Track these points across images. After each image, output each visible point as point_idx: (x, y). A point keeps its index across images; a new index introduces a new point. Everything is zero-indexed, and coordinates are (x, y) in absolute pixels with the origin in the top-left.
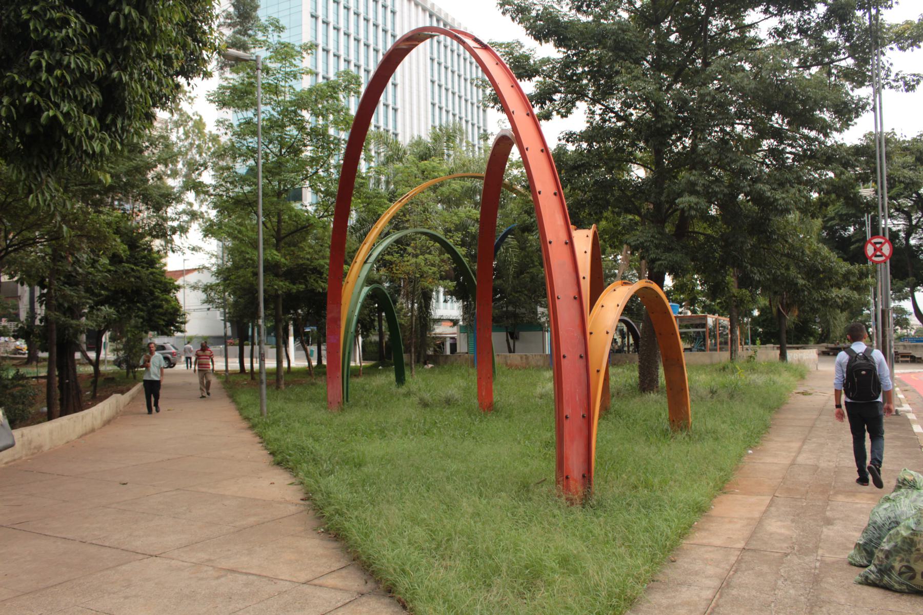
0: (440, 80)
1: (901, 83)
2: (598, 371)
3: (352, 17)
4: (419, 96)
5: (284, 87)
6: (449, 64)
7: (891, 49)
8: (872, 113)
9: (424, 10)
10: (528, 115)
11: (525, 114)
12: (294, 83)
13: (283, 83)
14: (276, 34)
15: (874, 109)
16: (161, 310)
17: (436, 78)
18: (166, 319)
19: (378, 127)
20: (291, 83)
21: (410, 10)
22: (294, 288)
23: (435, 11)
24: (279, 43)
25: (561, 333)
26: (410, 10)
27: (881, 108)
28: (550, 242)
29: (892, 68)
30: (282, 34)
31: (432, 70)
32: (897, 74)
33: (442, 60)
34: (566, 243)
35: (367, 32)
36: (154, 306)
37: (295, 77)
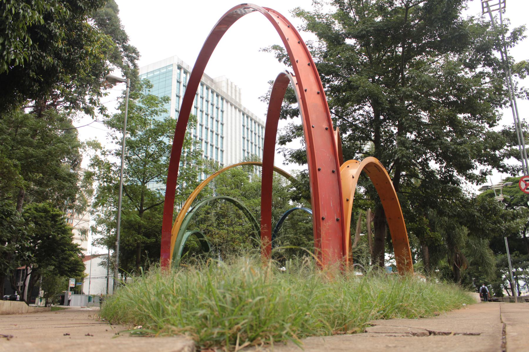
0: (248, 149)
1: (525, 94)
2: (347, 200)
3: (204, 130)
4: (231, 136)
5: (150, 120)
6: (253, 141)
7: (516, 76)
8: (510, 108)
9: (240, 111)
10: (289, 27)
11: (287, 27)
12: (156, 117)
13: (149, 118)
14: (147, 89)
15: (511, 105)
16: (67, 262)
17: (246, 148)
18: (70, 267)
19: (207, 157)
20: (154, 118)
21: (232, 111)
22: (148, 241)
23: (246, 112)
24: (149, 95)
25: (316, 152)
26: (232, 111)
27: (515, 104)
28: (306, 91)
29: (518, 86)
30: (151, 89)
31: (244, 144)
32: (521, 89)
33: (250, 139)
34: (318, 93)
35: (212, 138)
36: (63, 259)
37: (156, 114)
